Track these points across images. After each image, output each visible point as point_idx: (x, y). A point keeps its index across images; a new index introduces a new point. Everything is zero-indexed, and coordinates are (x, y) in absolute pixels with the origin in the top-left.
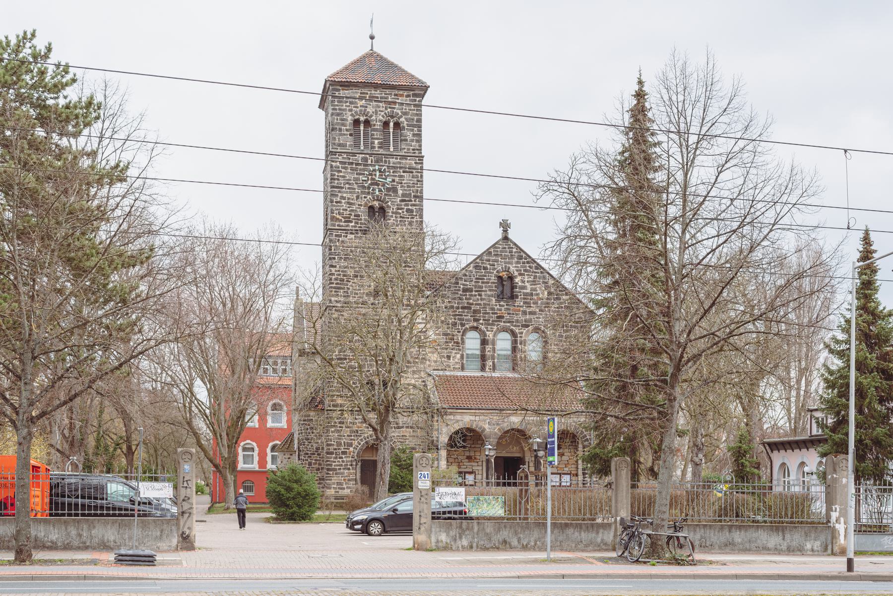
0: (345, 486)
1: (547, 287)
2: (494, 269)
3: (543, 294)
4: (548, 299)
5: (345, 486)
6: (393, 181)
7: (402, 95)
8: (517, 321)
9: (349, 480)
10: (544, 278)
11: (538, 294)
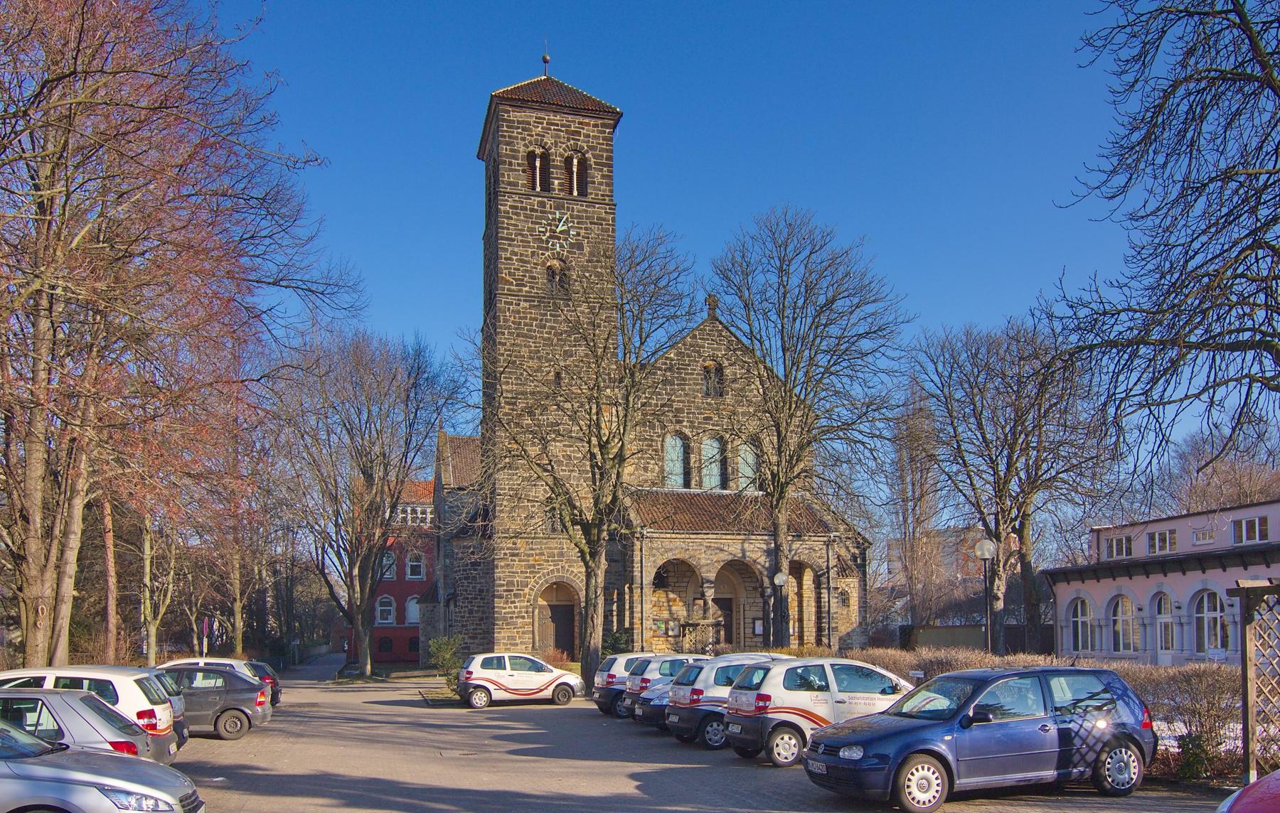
0: (518, 641)
6: (578, 234)
7: (588, 124)
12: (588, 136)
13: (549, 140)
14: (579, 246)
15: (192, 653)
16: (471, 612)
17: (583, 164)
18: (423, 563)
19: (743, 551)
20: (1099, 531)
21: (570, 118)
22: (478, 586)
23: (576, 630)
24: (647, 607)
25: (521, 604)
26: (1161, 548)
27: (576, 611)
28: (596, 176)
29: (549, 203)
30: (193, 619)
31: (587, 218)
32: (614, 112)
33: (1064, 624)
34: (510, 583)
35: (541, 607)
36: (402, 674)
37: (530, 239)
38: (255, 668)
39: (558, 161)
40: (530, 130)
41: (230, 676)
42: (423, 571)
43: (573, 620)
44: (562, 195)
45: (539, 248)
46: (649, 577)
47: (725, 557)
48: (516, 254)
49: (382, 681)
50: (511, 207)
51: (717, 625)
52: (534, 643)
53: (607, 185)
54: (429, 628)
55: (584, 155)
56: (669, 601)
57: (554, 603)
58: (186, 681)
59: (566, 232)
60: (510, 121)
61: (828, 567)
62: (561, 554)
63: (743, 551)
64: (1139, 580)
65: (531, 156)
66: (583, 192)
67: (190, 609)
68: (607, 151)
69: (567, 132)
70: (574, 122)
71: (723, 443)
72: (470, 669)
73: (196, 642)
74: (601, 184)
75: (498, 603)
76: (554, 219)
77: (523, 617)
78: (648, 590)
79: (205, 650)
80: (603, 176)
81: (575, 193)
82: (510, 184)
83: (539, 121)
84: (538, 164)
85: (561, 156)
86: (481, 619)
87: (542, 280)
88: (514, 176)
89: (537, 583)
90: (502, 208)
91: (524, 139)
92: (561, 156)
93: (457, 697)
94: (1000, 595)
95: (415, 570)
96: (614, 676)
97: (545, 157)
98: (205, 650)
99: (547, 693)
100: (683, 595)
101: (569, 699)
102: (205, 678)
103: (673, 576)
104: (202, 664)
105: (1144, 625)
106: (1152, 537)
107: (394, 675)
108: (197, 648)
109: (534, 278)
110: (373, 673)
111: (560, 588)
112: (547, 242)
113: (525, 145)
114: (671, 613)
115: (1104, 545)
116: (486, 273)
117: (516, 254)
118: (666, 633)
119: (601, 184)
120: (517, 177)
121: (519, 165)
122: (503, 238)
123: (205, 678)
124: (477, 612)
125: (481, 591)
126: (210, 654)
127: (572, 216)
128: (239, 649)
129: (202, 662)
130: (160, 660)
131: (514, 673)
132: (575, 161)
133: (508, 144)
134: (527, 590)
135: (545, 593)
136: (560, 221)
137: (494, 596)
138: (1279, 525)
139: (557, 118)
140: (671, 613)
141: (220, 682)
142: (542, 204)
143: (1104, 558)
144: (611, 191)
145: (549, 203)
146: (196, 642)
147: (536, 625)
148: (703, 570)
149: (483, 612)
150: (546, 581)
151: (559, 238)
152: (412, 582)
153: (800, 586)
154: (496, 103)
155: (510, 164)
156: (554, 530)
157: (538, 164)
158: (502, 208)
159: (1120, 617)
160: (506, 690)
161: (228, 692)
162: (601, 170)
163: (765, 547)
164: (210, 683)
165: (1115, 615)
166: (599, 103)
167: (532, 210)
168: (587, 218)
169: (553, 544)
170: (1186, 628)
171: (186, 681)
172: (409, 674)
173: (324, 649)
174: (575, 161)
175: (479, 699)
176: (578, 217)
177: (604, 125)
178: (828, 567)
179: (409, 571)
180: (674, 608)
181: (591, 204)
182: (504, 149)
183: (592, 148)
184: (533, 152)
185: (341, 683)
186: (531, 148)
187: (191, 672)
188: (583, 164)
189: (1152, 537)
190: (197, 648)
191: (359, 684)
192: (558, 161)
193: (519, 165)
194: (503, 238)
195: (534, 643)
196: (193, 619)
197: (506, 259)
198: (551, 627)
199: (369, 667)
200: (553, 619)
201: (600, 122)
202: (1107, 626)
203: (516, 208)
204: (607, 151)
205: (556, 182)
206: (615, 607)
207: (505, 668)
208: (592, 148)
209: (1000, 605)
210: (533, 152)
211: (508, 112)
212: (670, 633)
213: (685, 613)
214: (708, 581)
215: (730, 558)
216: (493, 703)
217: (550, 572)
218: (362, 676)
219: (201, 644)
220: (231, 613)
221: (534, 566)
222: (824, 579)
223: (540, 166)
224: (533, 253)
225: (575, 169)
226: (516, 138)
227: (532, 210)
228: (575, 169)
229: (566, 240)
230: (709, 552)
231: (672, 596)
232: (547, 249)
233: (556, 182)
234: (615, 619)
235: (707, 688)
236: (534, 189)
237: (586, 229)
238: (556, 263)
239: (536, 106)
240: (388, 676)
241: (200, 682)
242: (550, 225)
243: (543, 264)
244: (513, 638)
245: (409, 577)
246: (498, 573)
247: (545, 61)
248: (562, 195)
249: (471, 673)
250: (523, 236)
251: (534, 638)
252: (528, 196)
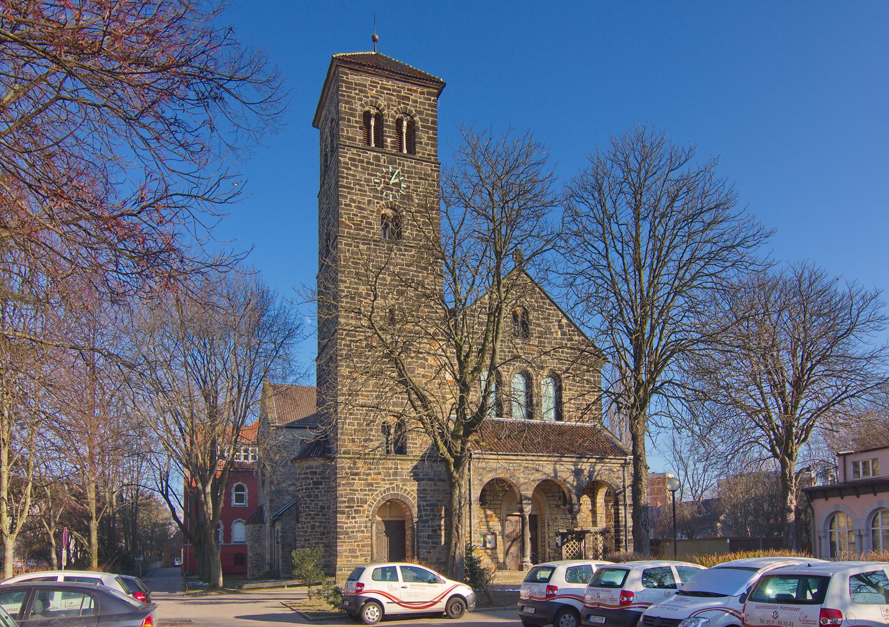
0: (358, 553)
1: (561, 327)
4: (561, 339)
5: (358, 553)
6: (408, 187)
7: (416, 91)
9: (363, 546)
10: (557, 316)
12: (416, 102)
13: (382, 103)
14: (409, 197)
15: (50, 567)
16: (313, 527)
17: (412, 125)
18: (246, 493)
19: (555, 471)
20: (845, 455)
21: (401, 84)
22: (320, 503)
23: (408, 543)
24: (475, 521)
25: (361, 519)
26: (865, 473)
27: (408, 526)
28: (423, 137)
29: (383, 158)
30: (51, 533)
31: (416, 173)
32: (438, 82)
33: (822, 535)
34: (351, 500)
35: (378, 523)
36: (253, 585)
37: (367, 188)
38: (126, 582)
39: (390, 121)
40: (366, 92)
41: (101, 595)
42: (246, 497)
43: (404, 534)
44: (394, 151)
45: (374, 197)
46: (476, 493)
47: (539, 476)
48: (354, 201)
49: (234, 592)
50: (350, 159)
51: (603, 533)
52: (372, 555)
53: (433, 146)
54: (256, 545)
55: (412, 118)
56: (487, 516)
57: (388, 519)
58: (38, 605)
59: (398, 185)
60: (348, 83)
61: (624, 487)
62: (395, 474)
63: (555, 471)
64: (850, 501)
65: (367, 116)
66: (411, 150)
67: (49, 525)
68: (432, 116)
69: (398, 96)
70: (405, 88)
71: (528, 377)
72: (361, 581)
73: (54, 556)
74: (427, 144)
75: (341, 518)
76: (387, 173)
77: (363, 532)
78: (476, 506)
79: (64, 563)
80: (429, 138)
81: (405, 151)
82: (348, 138)
83: (374, 85)
84: (373, 123)
85: (393, 117)
86: (323, 534)
87: (377, 227)
88: (352, 131)
89: (374, 500)
90: (342, 159)
91: (360, 100)
92: (393, 117)
93: (337, 610)
94: (793, 508)
95: (240, 498)
96: (555, 588)
97: (379, 118)
98: (64, 563)
99: (441, 606)
100: (498, 511)
101: (461, 613)
102: (64, 597)
103: (497, 494)
104: (61, 579)
105: (860, 536)
106: (856, 465)
107: (246, 586)
108: (55, 562)
109: (370, 224)
110: (224, 586)
111: (393, 505)
112: (382, 192)
113: (361, 105)
114: (489, 528)
115: (850, 468)
116: (321, 225)
117: (354, 201)
118: (485, 545)
119: (427, 144)
120: (355, 133)
121: (356, 122)
122: (343, 187)
123: (64, 597)
124: (319, 527)
125: (322, 508)
126: (69, 567)
127: (403, 171)
128: (95, 563)
129: (61, 576)
130: (17, 572)
131: (407, 584)
132: (405, 123)
133: (347, 102)
134: (366, 506)
135: (381, 509)
136: (392, 174)
137: (336, 512)
138: (888, 465)
139: (389, 84)
140: (489, 528)
141: (88, 603)
142: (377, 159)
143: (851, 477)
144: (436, 151)
145: (383, 158)
146: (54, 556)
147: (374, 538)
148: (522, 488)
149: (325, 527)
150: (383, 498)
151: (392, 190)
152: (235, 508)
153: (594, 504)
154: (337, 64)
155: (349, 121)
156: (388, 452)
157: (373, 123)
158: (342, 159)
159: (835, 530)
160: (399, 603)
161: (99, 619)
162: (427, 133)
163: (573, 468)
164: (76, 603)
165: (831, 528)
166: (425, 74)
167: (368, 163)
168: (416, 173)
169: (390, 464)
170: (864, 539)
171: (38, 605)
172: (260, 585)
173: (159, 564)
174: (405, 123)
175: (371, 614)
176: (408, 172)
177: (429, 93)
178: (624, 487)
179: (234, 498)
180: (491, 523)
181: (420, 161)
182: (343, 107)
183: (420, 113)
184: (368, 112)
185: (195, 595)
186: (367, 109)
187: (45, 591)
188: (412, 125)
189: (856, 465)
190: (55, 562)
191: (213, 595)
192: (390, 121)
193: (356, 122)
194: (343, 187)
195: (372, 555)
196: (51, 533)
197: (346, 205)
198: (385, 540)
199: (221, 579)
200: (387, 533)
201: (426, 90)
202: (867, 535)
203: (354, 160)
204: (432, 116)
205: (389, 140)
206: (443, 522)
207: (397, 580)
208: (420, 113)
209: (792, 517)
210: (368, 112)
211: (347, 74)
212: (488, 546)
213: (500, 528)
214: (527, 498)
215: (544, 477)
216: (385, 618)
217: (384, 489)
218: (214, 587)
219: (59, 557)
220: (87, 532)
221: (372, 485)
222: (621, 497)
223: (374, 124)
224: (369, 202)
225: (404, 131)
226: (354, 98)
227: (368, 163)
228: (404, 131)
229: (398, 191)
230: (527, 472)
231: (489, 512)
232: (381, 199)
233: (389, 140)
234: (443, 533)
235: (845, 606)
236: (369, 144)
237: (416, 183)
238: (389, 212)
239: (371, 70)
240: (240, 587)
241: (58, 602)
242: (384, 177)
243: (379, 211)
244: (354, 551)
245: (234, 503)
246: (341, 490)
247: (374, 40)
248: (394, 151)
249: (363, 585)
250: (360, 185)
251: (372, 550)
252: (365, 150)
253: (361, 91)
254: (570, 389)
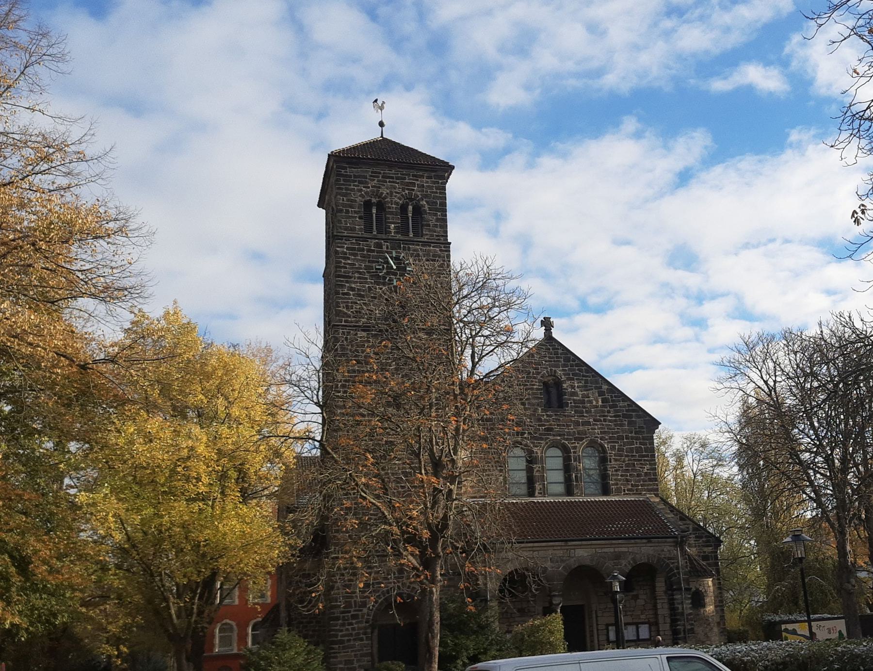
2: (538, 373)
3: (597, 402)
4: (602, 406)
7: (422, 176)
8: (569, 434)
11: (591, 402)
13: (385, 191)
65: (368, 205)
155: (347, 212)
162: (436, 215)
253: (360, 182)
254: (616, 460)
